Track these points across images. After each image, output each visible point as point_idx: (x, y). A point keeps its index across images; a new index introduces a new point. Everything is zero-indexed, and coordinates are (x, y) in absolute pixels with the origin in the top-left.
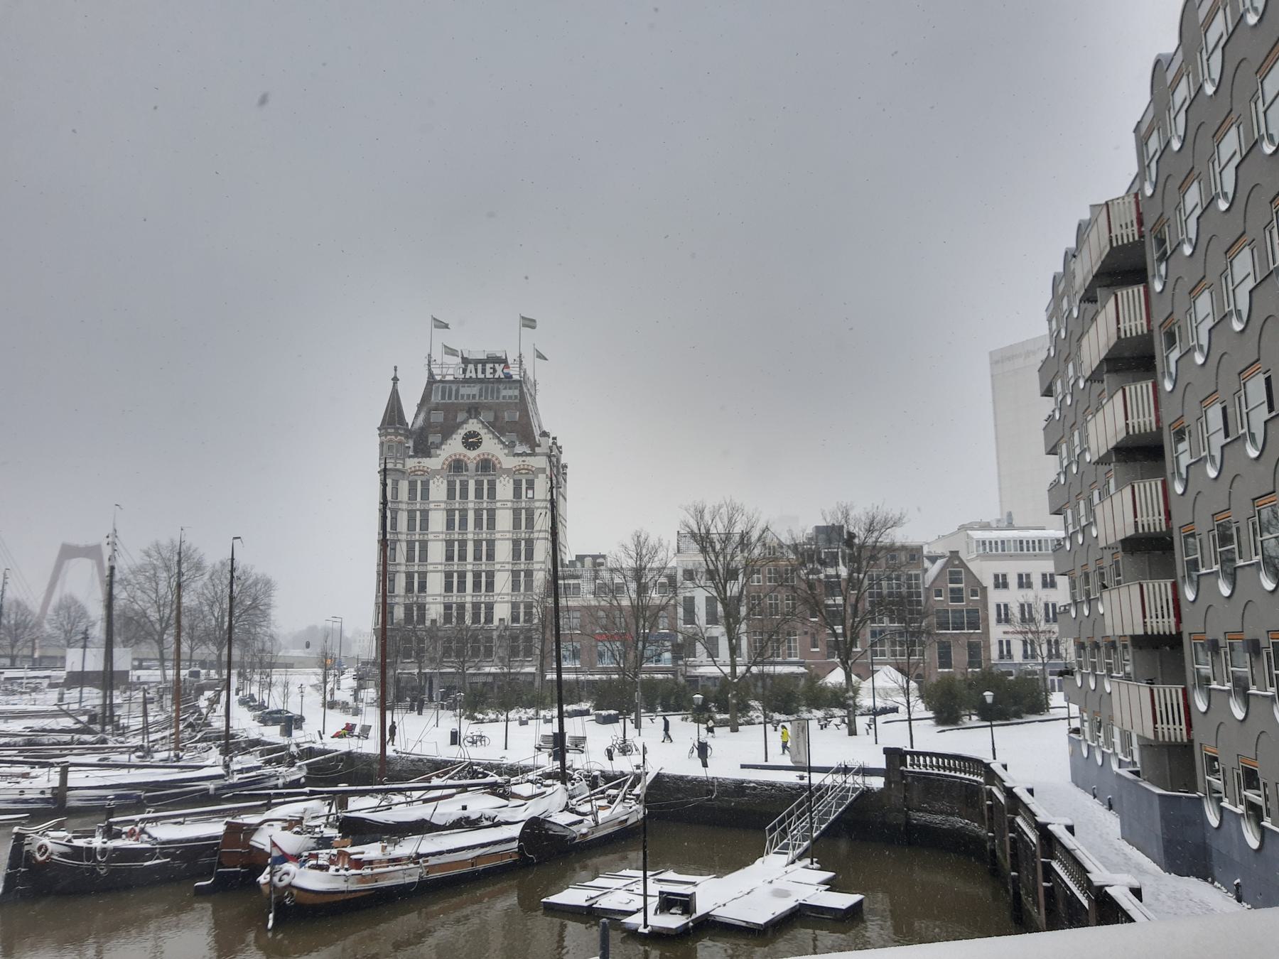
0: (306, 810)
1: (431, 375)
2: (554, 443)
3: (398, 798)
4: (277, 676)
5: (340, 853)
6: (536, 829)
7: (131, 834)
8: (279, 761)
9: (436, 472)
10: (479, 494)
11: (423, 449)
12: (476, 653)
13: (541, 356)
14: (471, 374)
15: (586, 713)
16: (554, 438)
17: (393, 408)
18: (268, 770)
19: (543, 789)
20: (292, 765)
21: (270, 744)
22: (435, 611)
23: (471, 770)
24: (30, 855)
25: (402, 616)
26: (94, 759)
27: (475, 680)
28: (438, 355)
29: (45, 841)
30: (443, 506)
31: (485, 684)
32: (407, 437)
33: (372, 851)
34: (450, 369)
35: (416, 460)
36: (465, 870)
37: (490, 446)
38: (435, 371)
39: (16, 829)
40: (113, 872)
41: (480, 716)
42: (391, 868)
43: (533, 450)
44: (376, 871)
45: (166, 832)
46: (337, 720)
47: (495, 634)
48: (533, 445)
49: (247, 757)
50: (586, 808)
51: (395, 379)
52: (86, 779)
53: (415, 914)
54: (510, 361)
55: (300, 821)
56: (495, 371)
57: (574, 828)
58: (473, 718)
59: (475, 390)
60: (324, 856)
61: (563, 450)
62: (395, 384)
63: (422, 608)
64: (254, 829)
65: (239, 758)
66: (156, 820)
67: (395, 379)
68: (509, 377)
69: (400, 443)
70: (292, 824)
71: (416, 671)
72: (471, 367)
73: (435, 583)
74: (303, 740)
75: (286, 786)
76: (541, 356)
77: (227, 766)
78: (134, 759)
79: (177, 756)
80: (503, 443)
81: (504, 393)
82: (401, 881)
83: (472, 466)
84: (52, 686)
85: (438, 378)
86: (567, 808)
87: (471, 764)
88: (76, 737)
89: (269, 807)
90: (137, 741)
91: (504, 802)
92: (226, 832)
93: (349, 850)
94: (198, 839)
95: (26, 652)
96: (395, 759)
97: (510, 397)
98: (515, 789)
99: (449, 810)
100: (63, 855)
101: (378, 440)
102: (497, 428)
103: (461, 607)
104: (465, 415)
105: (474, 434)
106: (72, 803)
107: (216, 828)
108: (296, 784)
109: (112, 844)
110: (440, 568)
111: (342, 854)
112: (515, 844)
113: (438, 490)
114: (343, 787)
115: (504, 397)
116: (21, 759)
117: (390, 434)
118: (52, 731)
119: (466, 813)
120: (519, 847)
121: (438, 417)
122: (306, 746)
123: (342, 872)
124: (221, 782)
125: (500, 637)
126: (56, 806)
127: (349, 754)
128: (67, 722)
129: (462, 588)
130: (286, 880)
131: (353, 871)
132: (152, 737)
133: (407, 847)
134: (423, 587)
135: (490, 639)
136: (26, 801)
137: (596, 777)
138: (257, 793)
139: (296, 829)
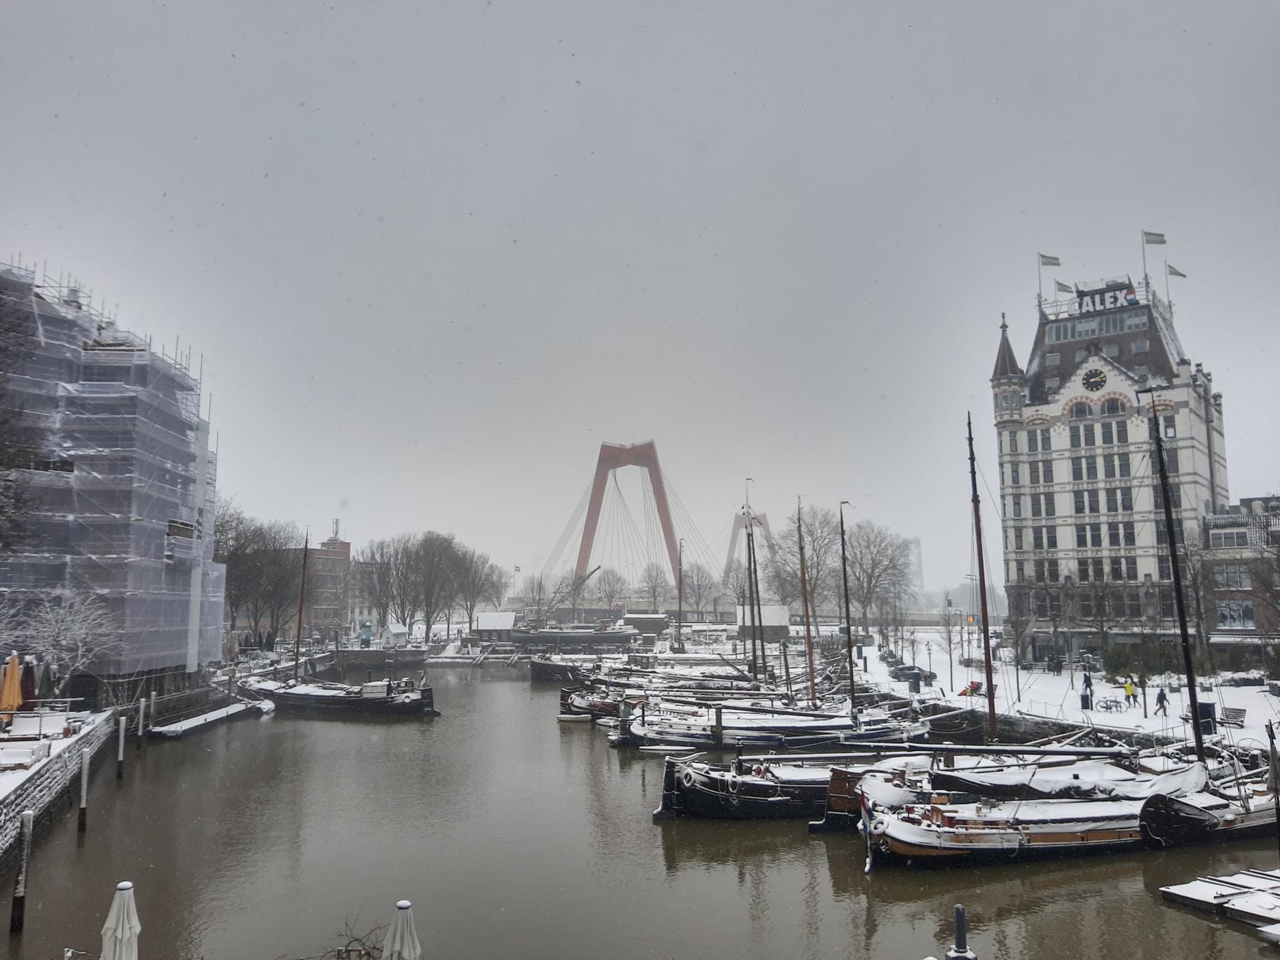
0: (907, 764)
1: (1043, 315)
2: (1199, 371)
3: (1012, 760)
4: (906, 632)
5: (934, 810)
6: (1161, 810)
7: (758, 772)
8: (904, 716)
9: (1056, 419)
10: (1107, 438)
11: (1040, 395)
12: (1119, 611)
13: (1174, 272)
14: (1088, 306)
15: (1258, 682)
16: (1198, 365)
17: (1004, 359)
18: (893, 724)
19: (1181, 765)
20: (915, 720)
21: (899, 699)
22: (1068, 566)
23: (1095, 736)
24: (679, 781)
25: (1033, 574)
26: (747, 703)
27: (1122, 640)
28: (1050, 293)
29: (690, 770)
30: (1067, 454)
31: (1134, 645)
32: (1021, 386)
33: (967, 811)
34: (1065, 306)
35: (1034, 408)
36: (1073, 843)
37: (1118, 384)
38: (1047, 311)
39: (667, 758)
40: (742, 802)
41: (1122, 680)
42: (987, 831)
43: (1170, 381)
44: (971, 831)
45: (786, 773)
46: (966, 677)
47: (1142, 592)
48: (1170, 375)
49: (877, 710)
50: (1233, 792)
51: (1004, 327)
52: (738, 721)
53: (1018, 882)
54: (1135, 285)
55: (901, 775)
56: (1116, 299)
57: (1214, 812)
58: (1115, 682)
59: (1093, 324)
60: (919, 809)
61: (1213, 377)
62: (1004, 331)
63: (1054, 564)
64: (858, 777)
65: (870, 711)
66: (777, 761)
67: (1004, 327)
68: (1134, 303)
69: (1015, 392)
70: (898, 777)
71: (1051, 630)
72: (1087, 299)
73: (1066, 538)
74: (928, 697)
75: (910, 740)
76: (1174, 272)
77: (855, 718)
78: (778, 704)
79: (814, 705)
80: (1132, 379)
81: (1129, 322)
82: (999, 846)
83: (1096, 408)
84: (729, 638)
85: (1052, 318)
86: (1206, 789)
87: (1095, 731)
88: (735, 683)
89: (878, 758)
90: (783, 690)
91: (1131, 775)
92: (833, 778)
93: (942, 807)
94: (814, 782)
95: (710, 608)
96: (1018, 720)
97: (1137, 326)
98: (1144, 762)
99: (1059, 778)
100: (703, 784)
101: (990, 393)
102: (1124, 362)
103: (1098, 562)
104: (1084, 353)
105: (1096, 373)
106: (728, 741)
107: (823, 774)
108: (919, 738)
109: (739, 779)
110: (1070, 521)
111: (934, 810)
112: (1136, 823)
113: (1060, 438)
114: (947, 745)
115: (1130, 327)
116: (693, 700)
117: (1004, 384)
118: (720, 677)
119: (1076, 783)
120: (1140, 826)
121: (1054, 360)
122: (932, 702)
123: (934, 827)
124: (850, 732)
125: (1147, 593)
126: (714, 745)
127: (972, 712)
128: (729, 670)
129: (1097, 541)
130: (881, 828)
131: (947, 829)
132: (795, 687)
133: (1005, 812)
134: (1053, 543)
135: (1135, 597)
136: (692, 736)
137: (1254, 757)
138: (877, 744)
139: (896, 782)
